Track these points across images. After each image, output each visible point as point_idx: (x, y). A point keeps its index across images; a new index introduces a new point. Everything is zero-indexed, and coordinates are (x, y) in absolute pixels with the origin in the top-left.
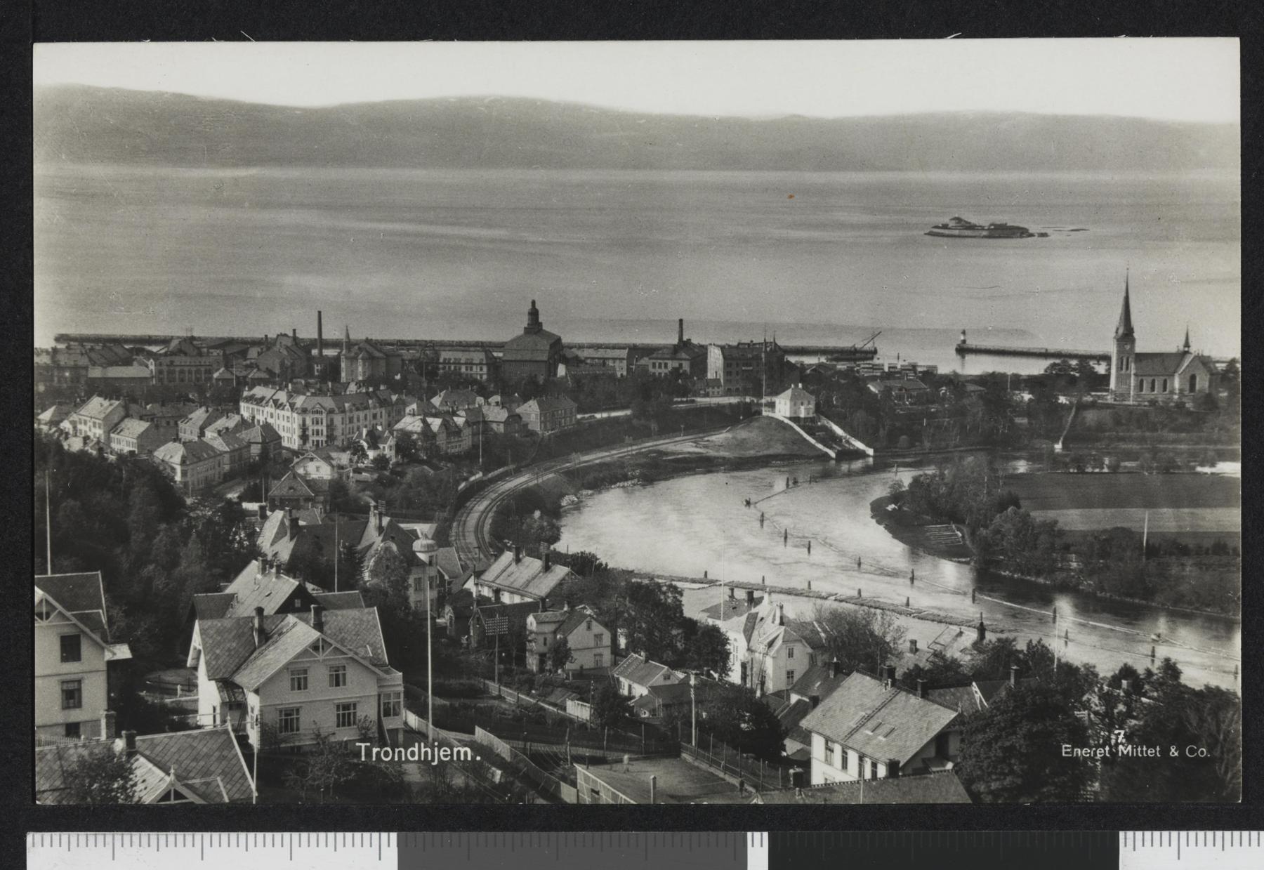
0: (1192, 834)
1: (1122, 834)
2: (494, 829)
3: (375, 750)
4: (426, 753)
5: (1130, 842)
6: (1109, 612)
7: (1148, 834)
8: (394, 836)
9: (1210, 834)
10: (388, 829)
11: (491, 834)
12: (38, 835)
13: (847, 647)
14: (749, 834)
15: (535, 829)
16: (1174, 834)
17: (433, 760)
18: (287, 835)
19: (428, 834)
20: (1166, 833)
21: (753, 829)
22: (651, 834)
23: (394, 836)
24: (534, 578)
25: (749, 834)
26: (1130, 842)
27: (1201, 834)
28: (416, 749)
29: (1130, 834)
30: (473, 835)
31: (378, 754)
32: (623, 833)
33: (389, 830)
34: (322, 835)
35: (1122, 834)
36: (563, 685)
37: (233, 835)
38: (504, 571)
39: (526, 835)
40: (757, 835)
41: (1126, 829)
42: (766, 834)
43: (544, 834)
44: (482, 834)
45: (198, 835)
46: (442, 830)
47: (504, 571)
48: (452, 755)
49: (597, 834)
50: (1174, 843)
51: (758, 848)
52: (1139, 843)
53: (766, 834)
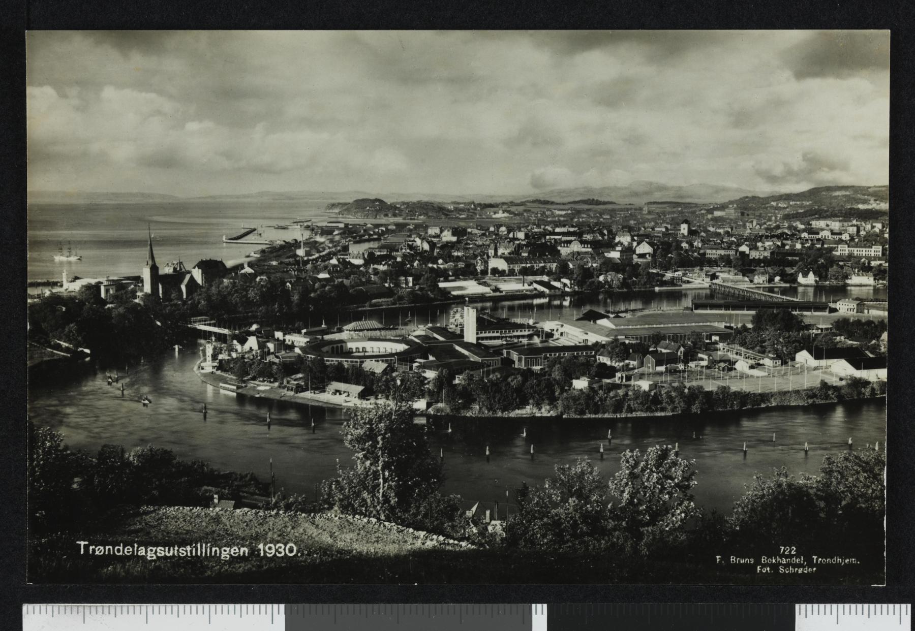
0: (847, 606)
2: (503, 602)
3: (91, 548)
5: (803, 611)
6: (526, 418)
7: (816, 606)
9: (860, 606)
10: (278, 602)
11: (351, 606)
12: (31, 606)
14: (534, 605)
15: (382, 601)
16: (834, 606)
18: (206, 606)
19: (307, 606)
20: (828, 606)
21: (537, 602)
22: (464, 605)
23: (282, 606)
24: (86, 242)
25: (534, 605)
26: (803, 611)
27: (853, 606)
28: (121, 548)
29: (803, 606)
30: (338, 606)
32: (444, 605)
33: (279, 602)
34: (232, 606)
35: (797, 606)
37: (169, 606)
39: (376, 606)
40: (539, 606)
42: (545, 606)
43: (388, 606)
44: (345, 606)
45: (144, 606)
46: (316, 602)
49: (426, 606)
51: (540, 615)
52: (809, 612)
53: (545, 606)
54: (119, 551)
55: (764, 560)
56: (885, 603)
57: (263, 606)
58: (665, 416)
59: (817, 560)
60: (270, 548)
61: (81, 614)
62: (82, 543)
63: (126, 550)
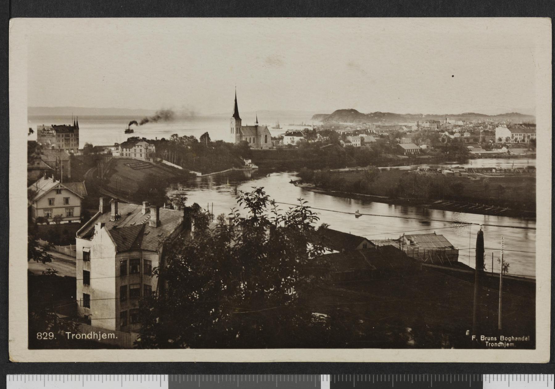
0: (515, 375)
1: (484, 375)
3: (73, 335)
4: (96, 336)
5: (488, 379)
8: (167, 376)
9: (522, 375)
12: (11, 376)
13: (456, 126)
14: (322, 375)
16: (507, 375)
17: (99, 338)
20: (503, 375)
23: (167, 376)
26: (488, 379)
28: (91, 335)
29: (488, 375)
31: (74, 337)
35: (484, 375)
36: (41, 246)
38: (513, 227)
40: (325, 376)
41: (486, 373)
47: (513, 227)
48: (107, 336)
50: (546, 379)
51: (325, 381)
52: (530, 379)
53: (329, 376)
54: (90, 336)
55: (502, 337)
56: (526, 373)
57: (116, 376)
58: (178, 168)
59: (70, 335)
60: (51, 335)
61: (43, 381)
62: (68, 333)
63: (103, 336)
